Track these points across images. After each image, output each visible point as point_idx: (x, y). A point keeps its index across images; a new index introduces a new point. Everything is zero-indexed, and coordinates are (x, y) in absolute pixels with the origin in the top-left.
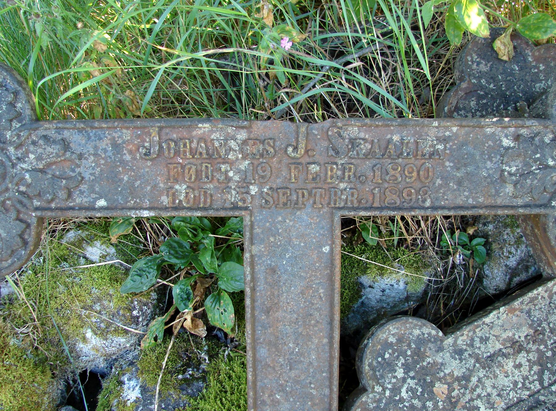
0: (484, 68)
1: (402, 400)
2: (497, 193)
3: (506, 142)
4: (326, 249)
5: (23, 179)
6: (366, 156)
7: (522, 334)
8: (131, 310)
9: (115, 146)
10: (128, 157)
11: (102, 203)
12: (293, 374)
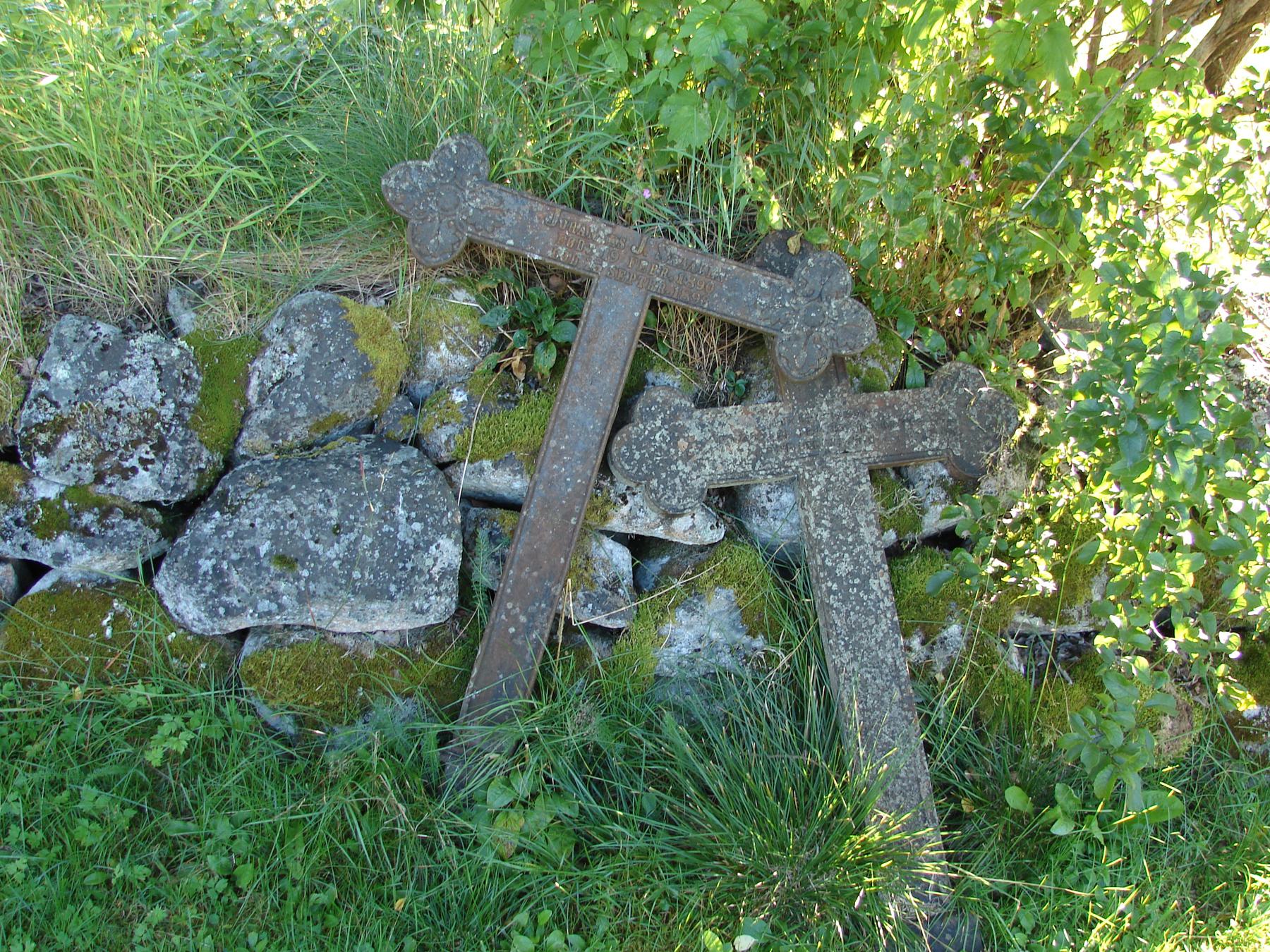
0: (776, 254)
1: (655, 441)
2: (750, 314)
3: (763, 285)
4: (637, 314)
5: (467, 211)
6: (677, 266)
7: (750, 431)
8: (479, 339)
9: (532, 212)
10: (536, 221)
11: (511, 242)
12: (592, 388)
